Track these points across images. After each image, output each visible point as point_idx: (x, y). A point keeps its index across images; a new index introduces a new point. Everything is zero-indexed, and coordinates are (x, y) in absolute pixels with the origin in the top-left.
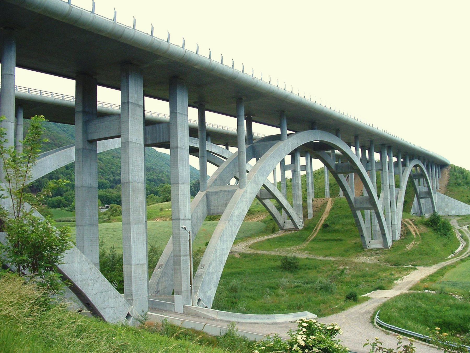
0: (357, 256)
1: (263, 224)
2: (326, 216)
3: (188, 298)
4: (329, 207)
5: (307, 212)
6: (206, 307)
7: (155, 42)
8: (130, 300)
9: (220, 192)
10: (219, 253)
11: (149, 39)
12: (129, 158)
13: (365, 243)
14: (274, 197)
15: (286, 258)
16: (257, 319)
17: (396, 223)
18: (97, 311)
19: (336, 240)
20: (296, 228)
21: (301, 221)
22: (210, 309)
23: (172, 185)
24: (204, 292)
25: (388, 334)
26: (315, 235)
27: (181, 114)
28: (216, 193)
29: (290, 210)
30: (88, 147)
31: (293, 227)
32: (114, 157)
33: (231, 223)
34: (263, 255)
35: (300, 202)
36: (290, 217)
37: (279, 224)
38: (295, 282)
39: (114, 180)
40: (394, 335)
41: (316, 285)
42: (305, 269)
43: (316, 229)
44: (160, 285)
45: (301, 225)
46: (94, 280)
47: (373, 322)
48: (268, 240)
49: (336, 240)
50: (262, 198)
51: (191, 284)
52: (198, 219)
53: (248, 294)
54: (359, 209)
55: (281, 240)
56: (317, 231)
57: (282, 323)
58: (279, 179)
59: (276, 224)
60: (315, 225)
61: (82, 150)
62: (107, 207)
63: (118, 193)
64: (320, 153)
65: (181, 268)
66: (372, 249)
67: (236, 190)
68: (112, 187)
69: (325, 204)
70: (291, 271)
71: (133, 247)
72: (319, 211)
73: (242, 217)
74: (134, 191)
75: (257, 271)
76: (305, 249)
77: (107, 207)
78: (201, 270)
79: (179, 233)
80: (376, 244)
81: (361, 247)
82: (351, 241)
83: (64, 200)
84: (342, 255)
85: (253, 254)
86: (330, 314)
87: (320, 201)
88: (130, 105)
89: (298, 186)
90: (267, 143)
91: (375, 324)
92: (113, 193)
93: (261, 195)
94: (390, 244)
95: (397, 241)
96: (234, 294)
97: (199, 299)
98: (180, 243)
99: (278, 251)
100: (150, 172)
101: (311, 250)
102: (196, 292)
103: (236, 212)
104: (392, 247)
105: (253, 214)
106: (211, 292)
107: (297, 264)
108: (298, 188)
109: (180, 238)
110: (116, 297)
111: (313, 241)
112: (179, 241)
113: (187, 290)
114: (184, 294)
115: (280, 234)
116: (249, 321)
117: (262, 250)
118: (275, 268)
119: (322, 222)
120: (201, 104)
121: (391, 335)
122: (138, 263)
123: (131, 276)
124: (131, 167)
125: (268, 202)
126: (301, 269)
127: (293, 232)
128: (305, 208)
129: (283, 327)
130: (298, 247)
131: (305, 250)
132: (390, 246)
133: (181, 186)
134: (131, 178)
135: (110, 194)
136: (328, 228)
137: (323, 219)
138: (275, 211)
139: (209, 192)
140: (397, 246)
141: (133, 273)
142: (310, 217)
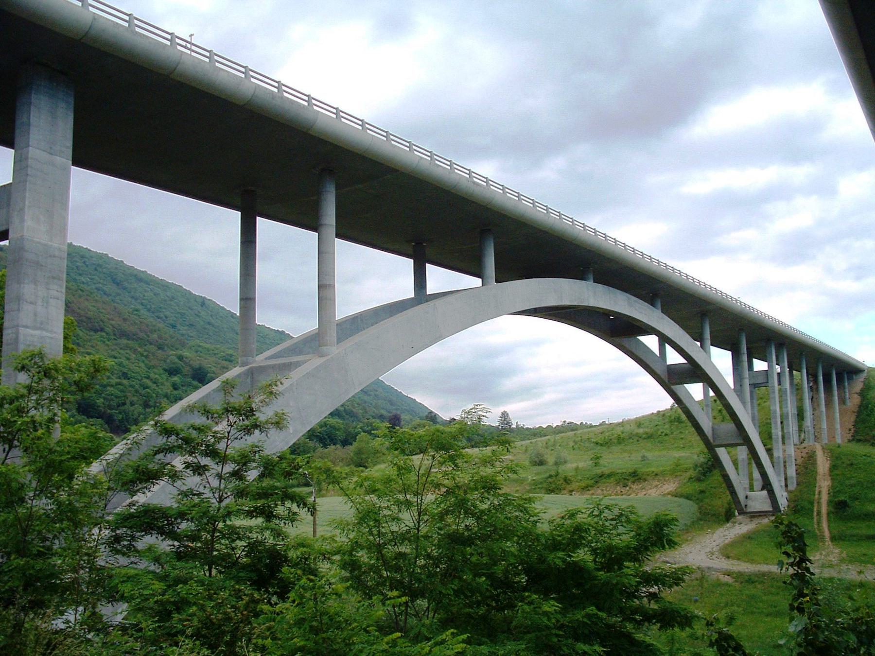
43: (819, 513)
93: (714, 438)
105: (645, 480)
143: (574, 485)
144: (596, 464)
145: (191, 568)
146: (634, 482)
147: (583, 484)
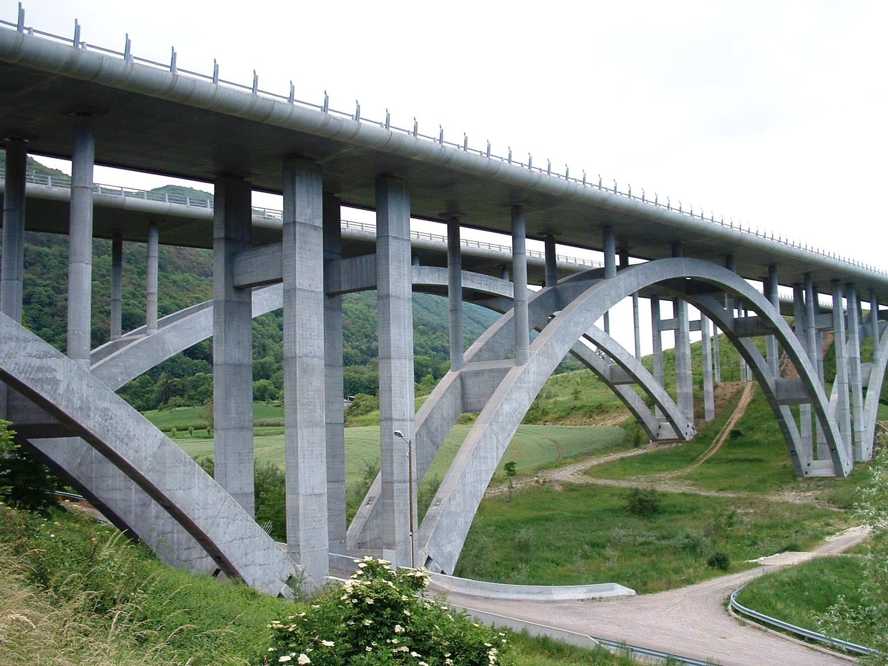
0: (779, 489)
1: (622, 430)
2: (740, 415)
3: (406, 554)
4: (746, 398)
5: (703, 408)
6: (443, 572)
7: (331, 121)
8: (294, 555)
9: (483, 371)
10: (469, 479)
11: (321, 118)
12: (295, 316)
13: (799, 466)
14: (635, 380)
15: (636, 492)
16: (518, 592)
17: (862, 429)
18: (234, 569)
19: (750, 461)
20: (681, 438)
21: (691, 425)
22: (449, 575)
23: (381, 361)
24: (438, 546)
25: (744, 624)
26: (714, 451)
27: (396, 238)
28: (477, 373)
29: (668, 404)
30: (235, 297)
31: (673, 436)
32: (369, 306)
33: (495, 427)
34: (605, 487)
35: (689, 389)
36: (669, 418)
37: (648, 431)
38: (643, 536)
39: (369, 348)
40: (754, 627)
41: (680, 540)
42: (672, 513)
43: (718, 440)
44: (368, 533)
45: (689, 431)
46: (227, 517)
47: (726, 605)
48: (622, 459)
49: (750, 461)
50: (615, 381)
51: (411, 531)
52: (443, 419)
53: (549, 555)
54: (784, 402)
55: (647, 461)
56: (720, 444)
57: (564, 601)
58: (647, 349)
59: (643, 432)
60: (717, 433)
61: (223, 303)
62: (351, 399)
63: (373, 374)
64: (702, 299)
65: (393, 503)
66: (812, 478)
67: (510, 369)
68: (364, 363)
69: (739, 394)
70: (645, 516)
71: (301, 465)
72: (725, 406)
73: (519, 416)
74: (304, 371)
75: (581, 515)
76: (689, 477)
77: (351, 399)
78: (436, 507)
79: (392, 444)
80: (821, 468)
81: (793, 475)
82: (781, 462)
83: (272, 387)
84: (750, 488)
85: (587, 485)
86: (662, 590)
87: (729, 388)
88: (297, 227)
89: (684, 359)
90: (581, 283)
91: (729, 607)
92: (365, 373)
93: (612, 378)
94: (847, 467)
95: (863, 463)
96: (522, 554)
97: (429, 559)
98: (392, 460)
99: (634, 480)
100: (438, 334)
101: (697, 479)
102: (421, 546)
103: (507, 408)
104: (852, 475)
105: (607, 412)
106: (454, 547)
107: (656, 503)
108: (685, 363)
109: (392, 452)
110: (269, 548)
111: (708, 461)
112: (392, 456)
113: (406, 542)
114: (400, 547)
115: (650, 448)
116: (505, 596)
117: (606, 478)
118: (615, 511)
119: (731, 427)
120: (452, 218)
121: (748, 626)
122: (310, 491)
123: (297, 515)
124: (299, 331)
125: (626, 390)
126: (664, 512)
127: (674, 445)
128: (698, 400)
129: (565, 608)
130: (676, 473)
131: (686, 479)
132: (848, 472)
133: (395, 363)
134: (300, 350)
135: (356, 376)
136: (739, 438)
137: (733, 422)
138: (640, 407)
139: (465, 373)
140: (860, 474)
141: (301, 510)
142: (709, 418)
143: (551, 416)
144: (576, 398)
145: (521, 560)
146: (598, 414)
147: (556, 416)
